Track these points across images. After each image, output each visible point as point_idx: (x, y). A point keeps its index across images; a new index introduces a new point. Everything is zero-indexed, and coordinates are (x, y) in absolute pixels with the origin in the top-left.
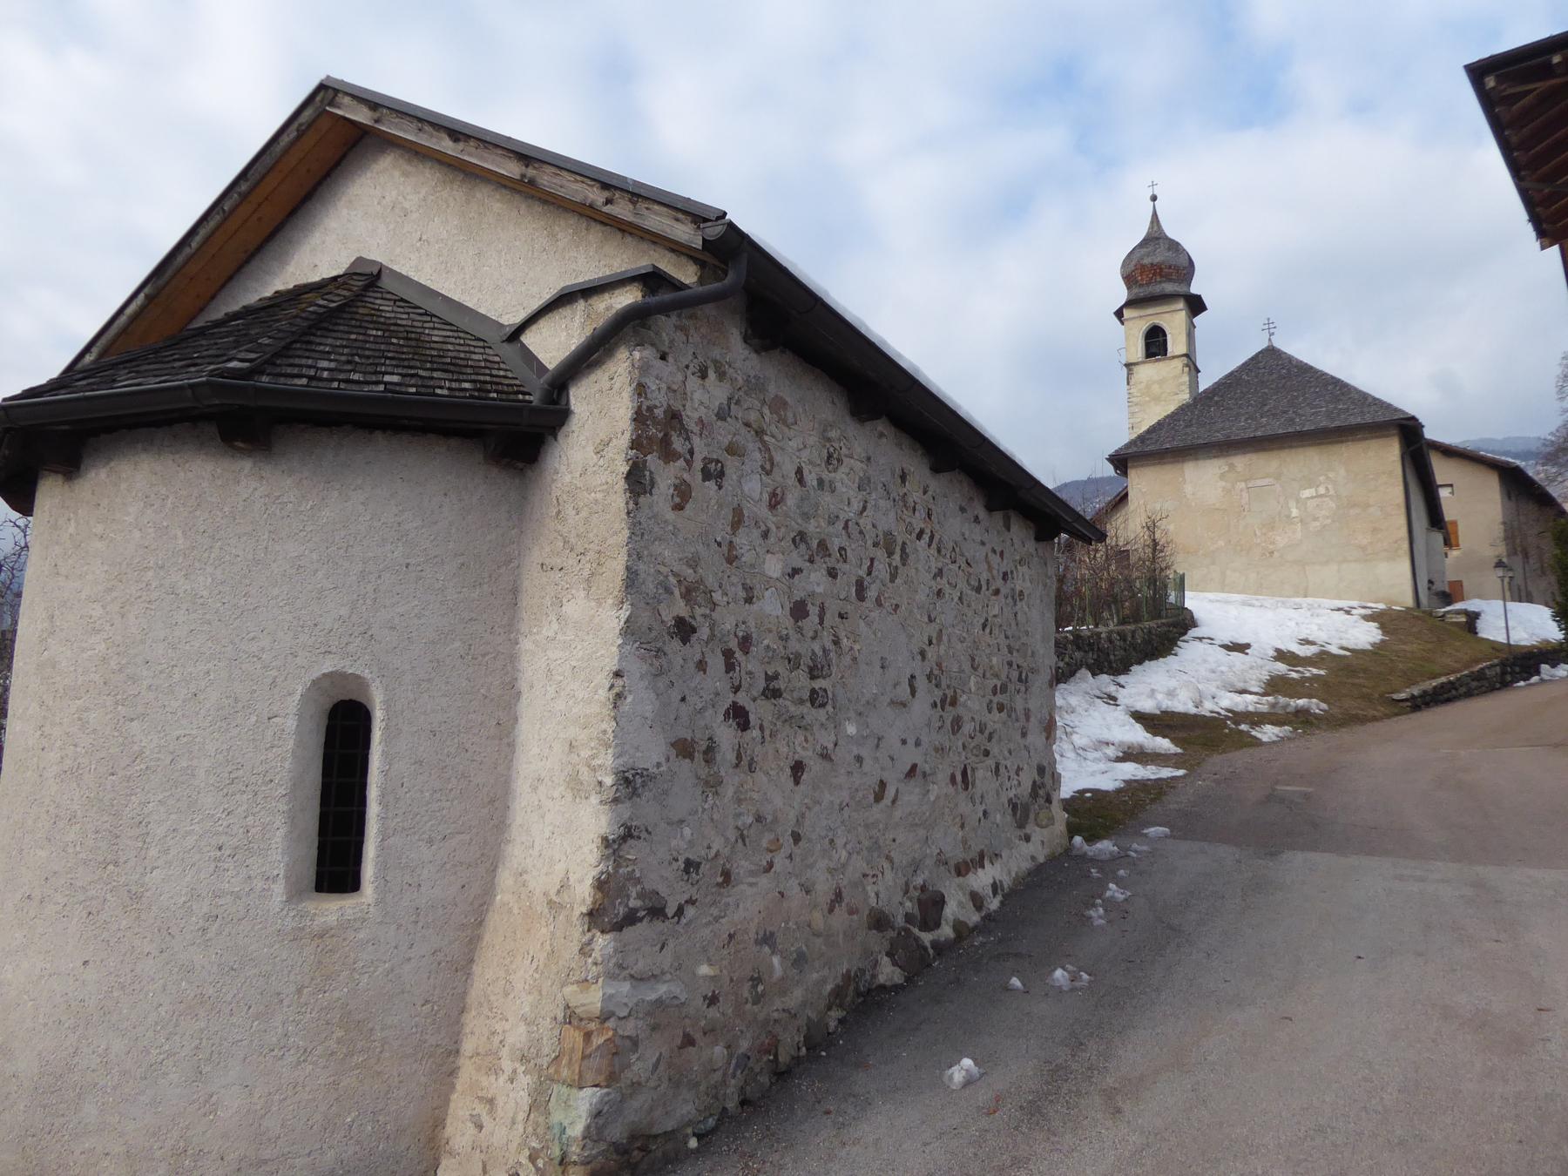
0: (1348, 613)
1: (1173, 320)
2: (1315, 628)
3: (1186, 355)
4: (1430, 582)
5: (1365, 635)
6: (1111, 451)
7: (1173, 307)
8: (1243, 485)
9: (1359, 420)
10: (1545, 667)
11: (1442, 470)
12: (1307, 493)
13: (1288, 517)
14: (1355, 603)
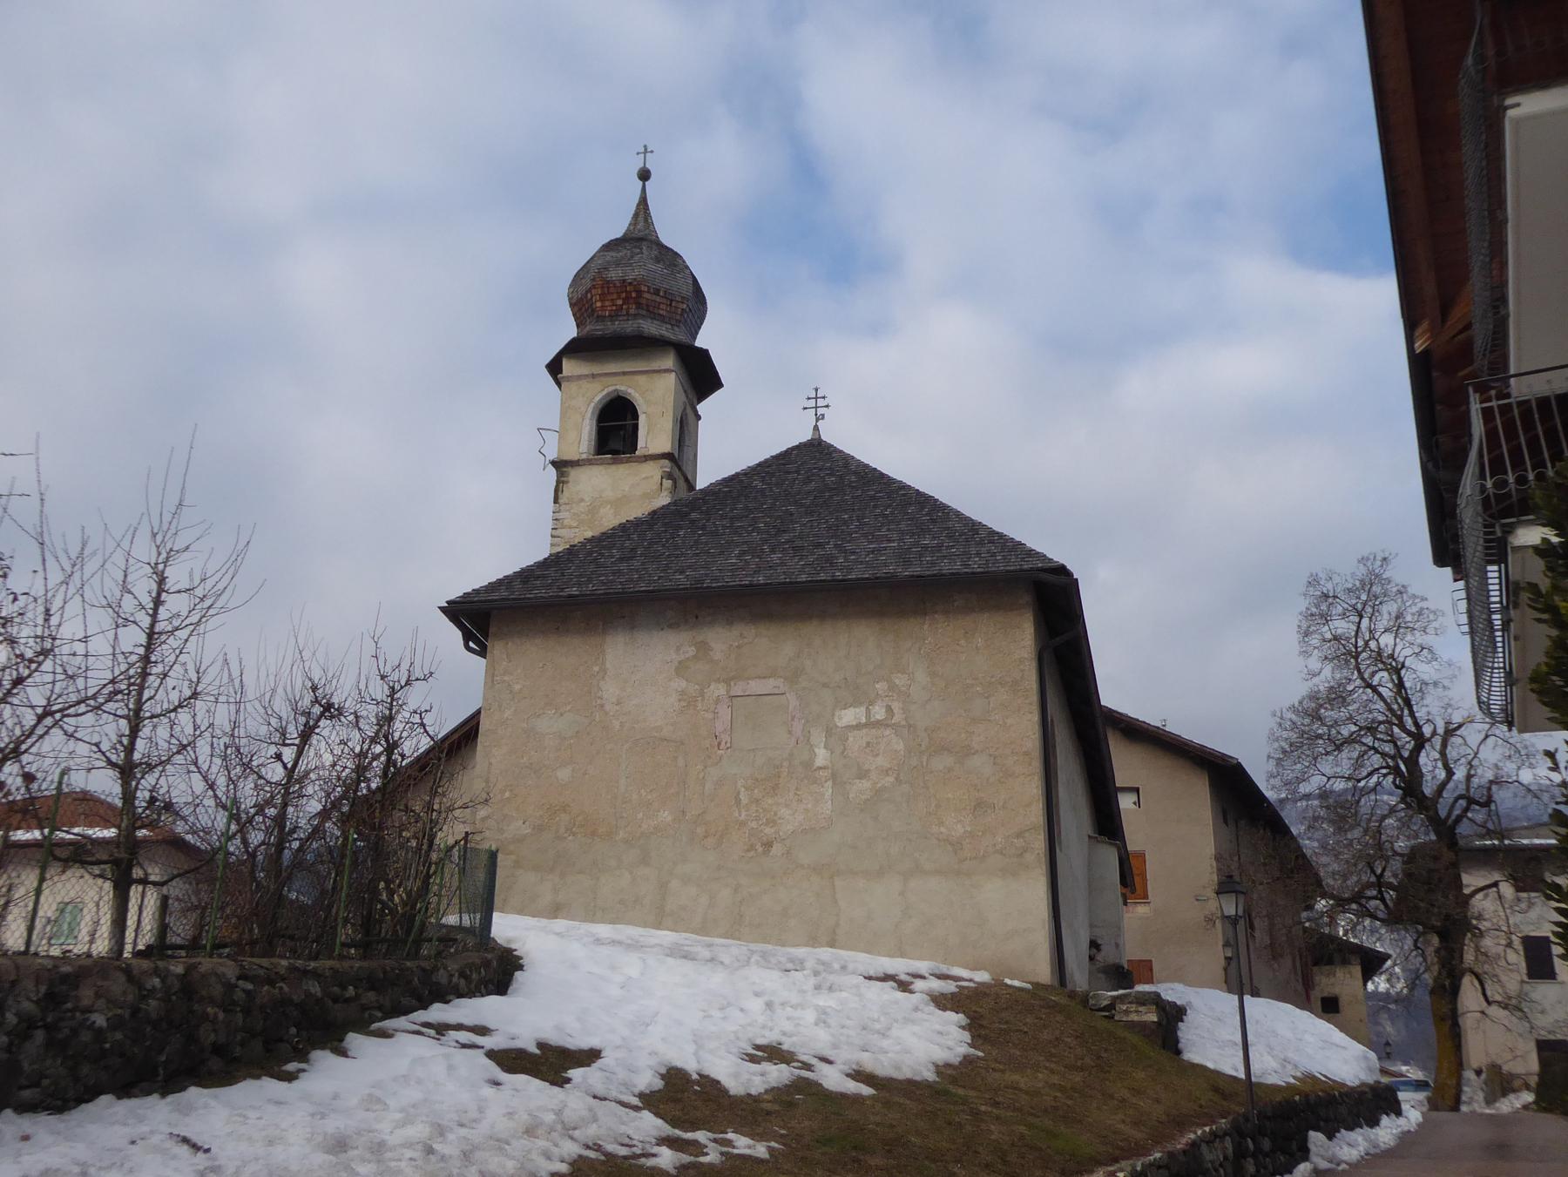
0: (904, 986)
1: (655, 391)
2: (810, 1016)
3: (668, 456)
4: (1094, 945)
5: (925, 1041)
6: (455, 593)
8: (718, 690)
9: (957, 567)
10: (1316, 1138)
11: (1126, 764)
12: (849, 716)
13: (808, 764)
14: (923, 966)
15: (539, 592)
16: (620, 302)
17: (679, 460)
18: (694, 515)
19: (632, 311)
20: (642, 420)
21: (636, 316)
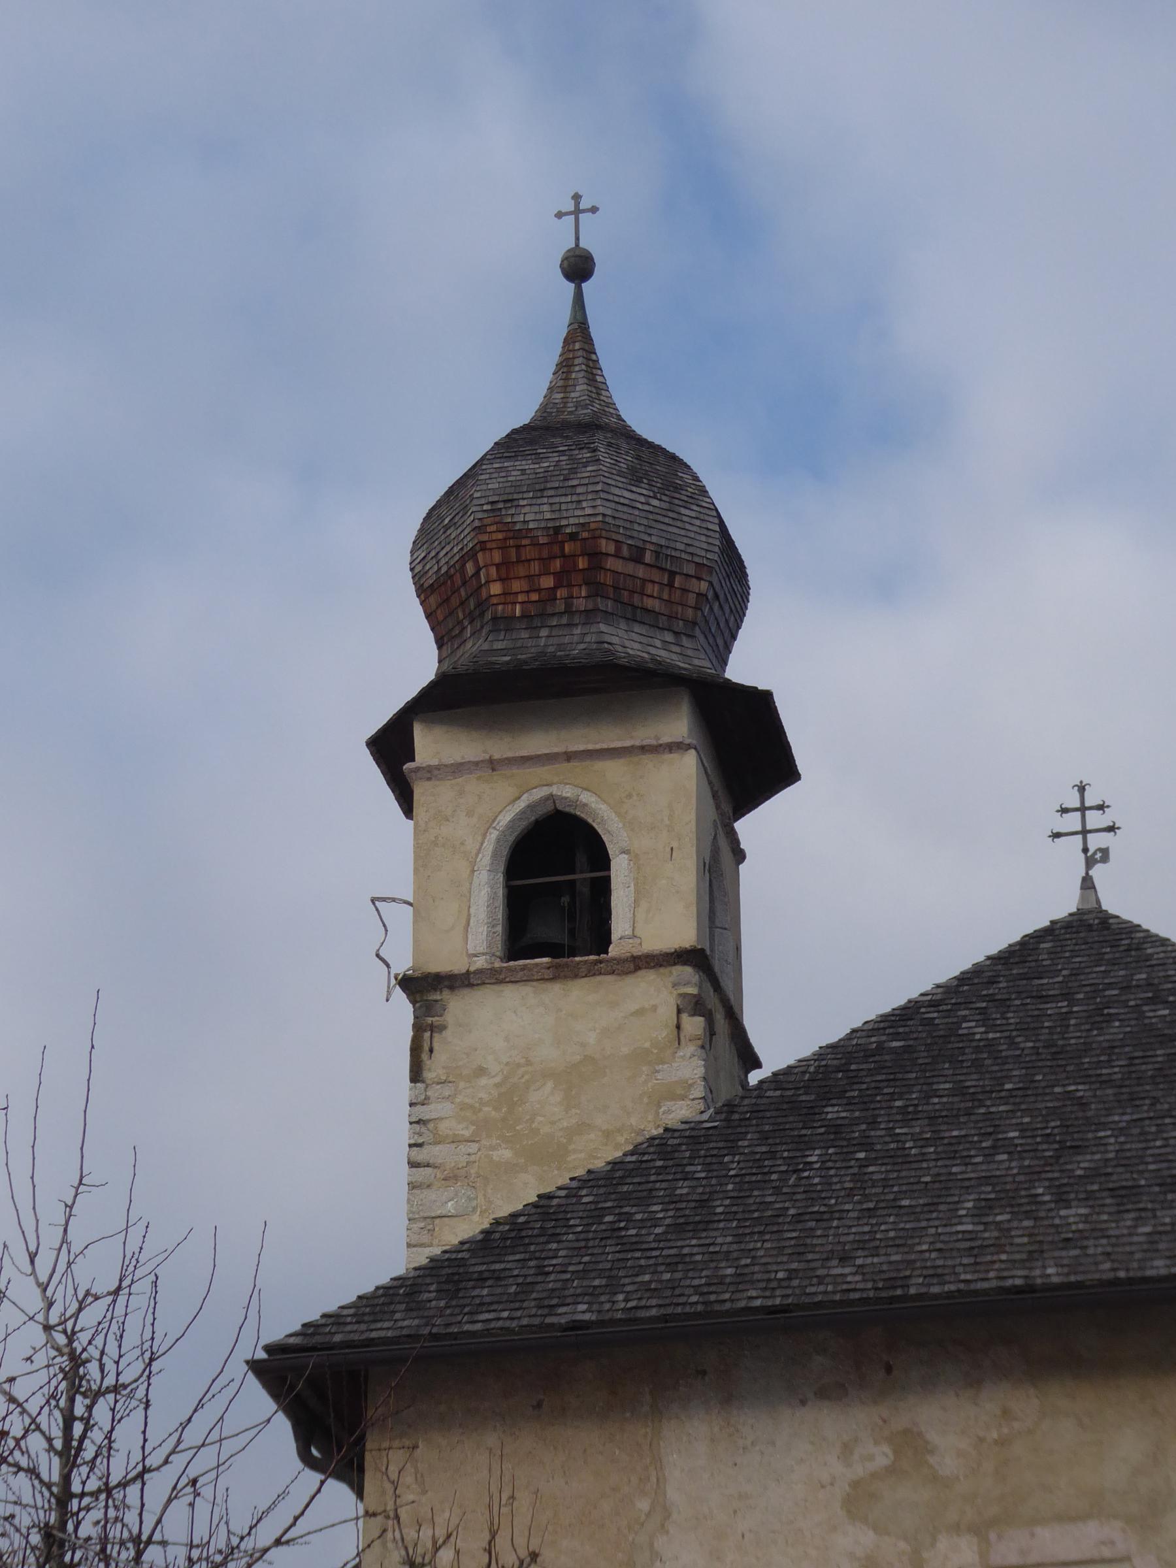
1: (642, 795)
6: (282, 1323)
7: (644, 734)
15: (491, 1318)
16: (548, 582)
17: (709, 973)
18: (833, 1112)
19: (580, 604)
20: (620, 870)
21: (590, 615)
